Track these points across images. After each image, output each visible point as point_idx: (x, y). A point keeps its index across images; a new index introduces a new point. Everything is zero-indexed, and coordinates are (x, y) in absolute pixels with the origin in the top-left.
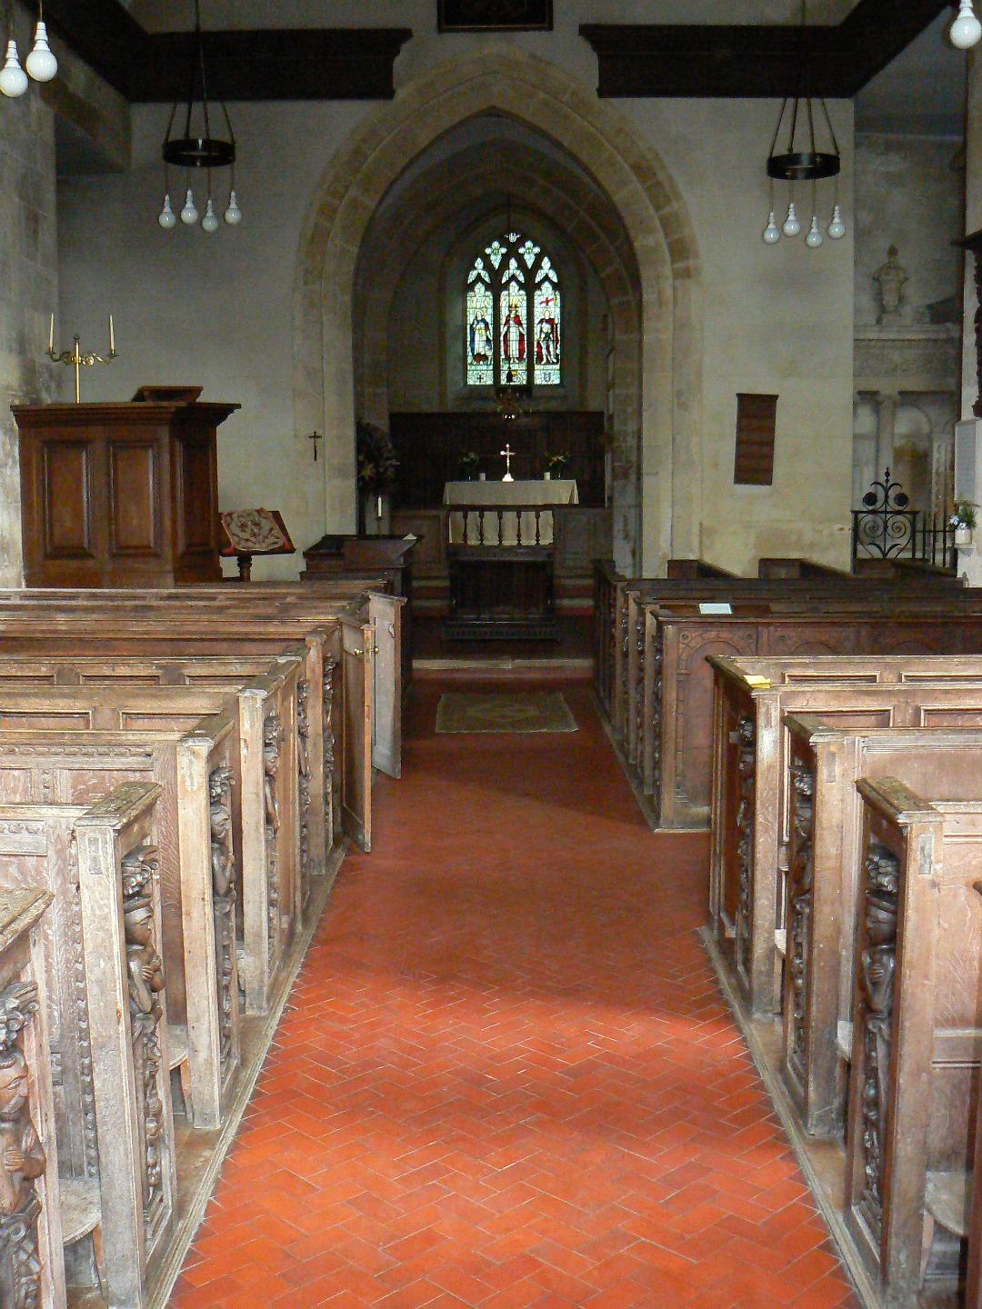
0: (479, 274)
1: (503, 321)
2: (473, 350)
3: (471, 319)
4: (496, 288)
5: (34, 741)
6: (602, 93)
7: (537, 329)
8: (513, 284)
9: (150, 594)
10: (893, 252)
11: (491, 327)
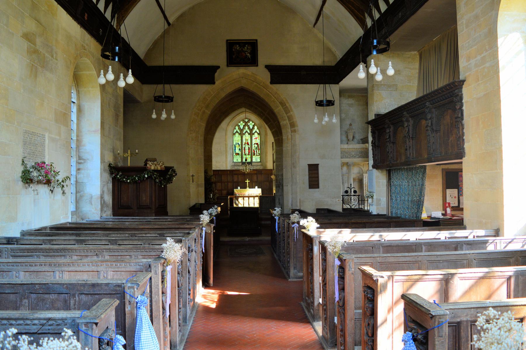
0: (237, 131)
1: (244, 144)
2: (235, 152)
3: (234, 143)
4: (242, 134)
5: (133, 248)
6: (272, 82)
7: (253, 146)
8: (247, 133)
9: (149, 218)
10: (351, 125)
11: (240, 145)
